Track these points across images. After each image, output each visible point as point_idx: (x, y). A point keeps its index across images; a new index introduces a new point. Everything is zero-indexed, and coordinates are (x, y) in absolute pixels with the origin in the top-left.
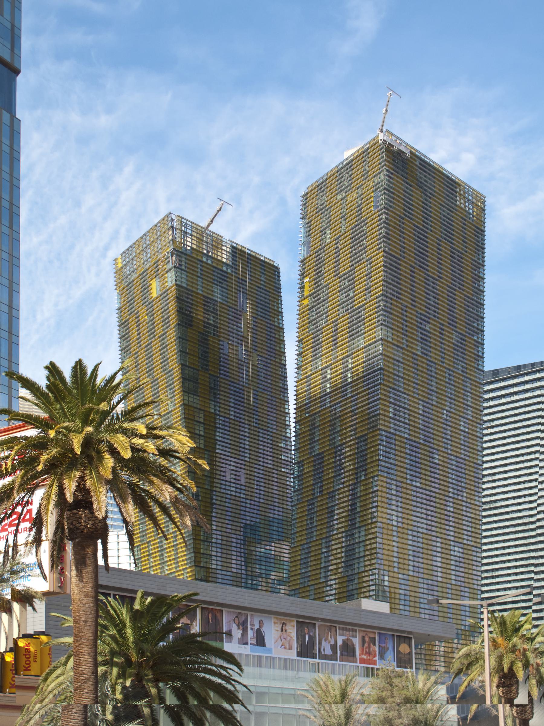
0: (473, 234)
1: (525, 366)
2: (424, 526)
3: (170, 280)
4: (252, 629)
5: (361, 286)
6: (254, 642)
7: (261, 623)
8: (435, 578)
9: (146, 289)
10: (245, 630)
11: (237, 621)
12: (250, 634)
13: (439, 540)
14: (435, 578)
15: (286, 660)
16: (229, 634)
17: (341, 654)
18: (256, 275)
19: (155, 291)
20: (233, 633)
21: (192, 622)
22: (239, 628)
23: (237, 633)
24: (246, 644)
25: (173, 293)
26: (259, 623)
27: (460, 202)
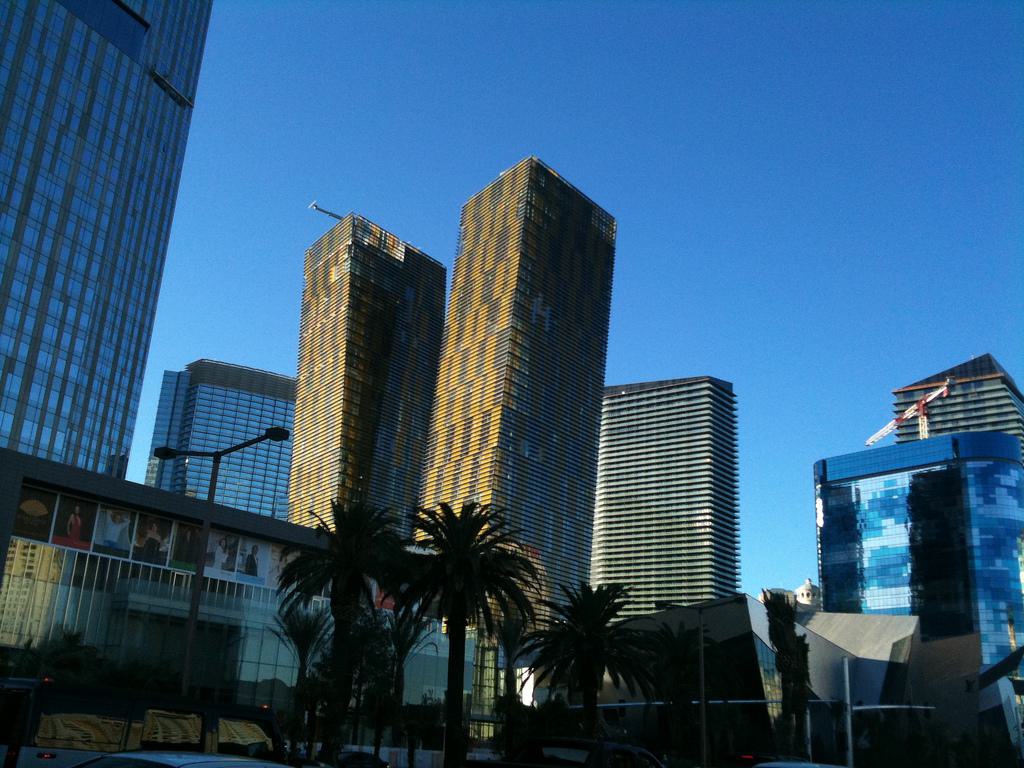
0: (604, 253)
1: (667, 382)
2: (538, 498)
3: (346, 267)
4: (242, 555)
5: (499, 281)
6: (243, 569)
7: (255, 550)
8: (545, 549)
9: (327, 274)
10: (233, 555)
11: (223, 543)
12: (239, 559)
13: (551, 513)
14: (545, 549)
15: (223, 583)
16: (211, 557)
17: (53, 539)
18: (424, 274)
19: (334, 278)
20: (217, 557)
21: (163, 539)
22: (225, 552)
23: (221, 557)
24: (232, 570)
25: (347, 279)
26: (253, 548)
27: (594, 222)
